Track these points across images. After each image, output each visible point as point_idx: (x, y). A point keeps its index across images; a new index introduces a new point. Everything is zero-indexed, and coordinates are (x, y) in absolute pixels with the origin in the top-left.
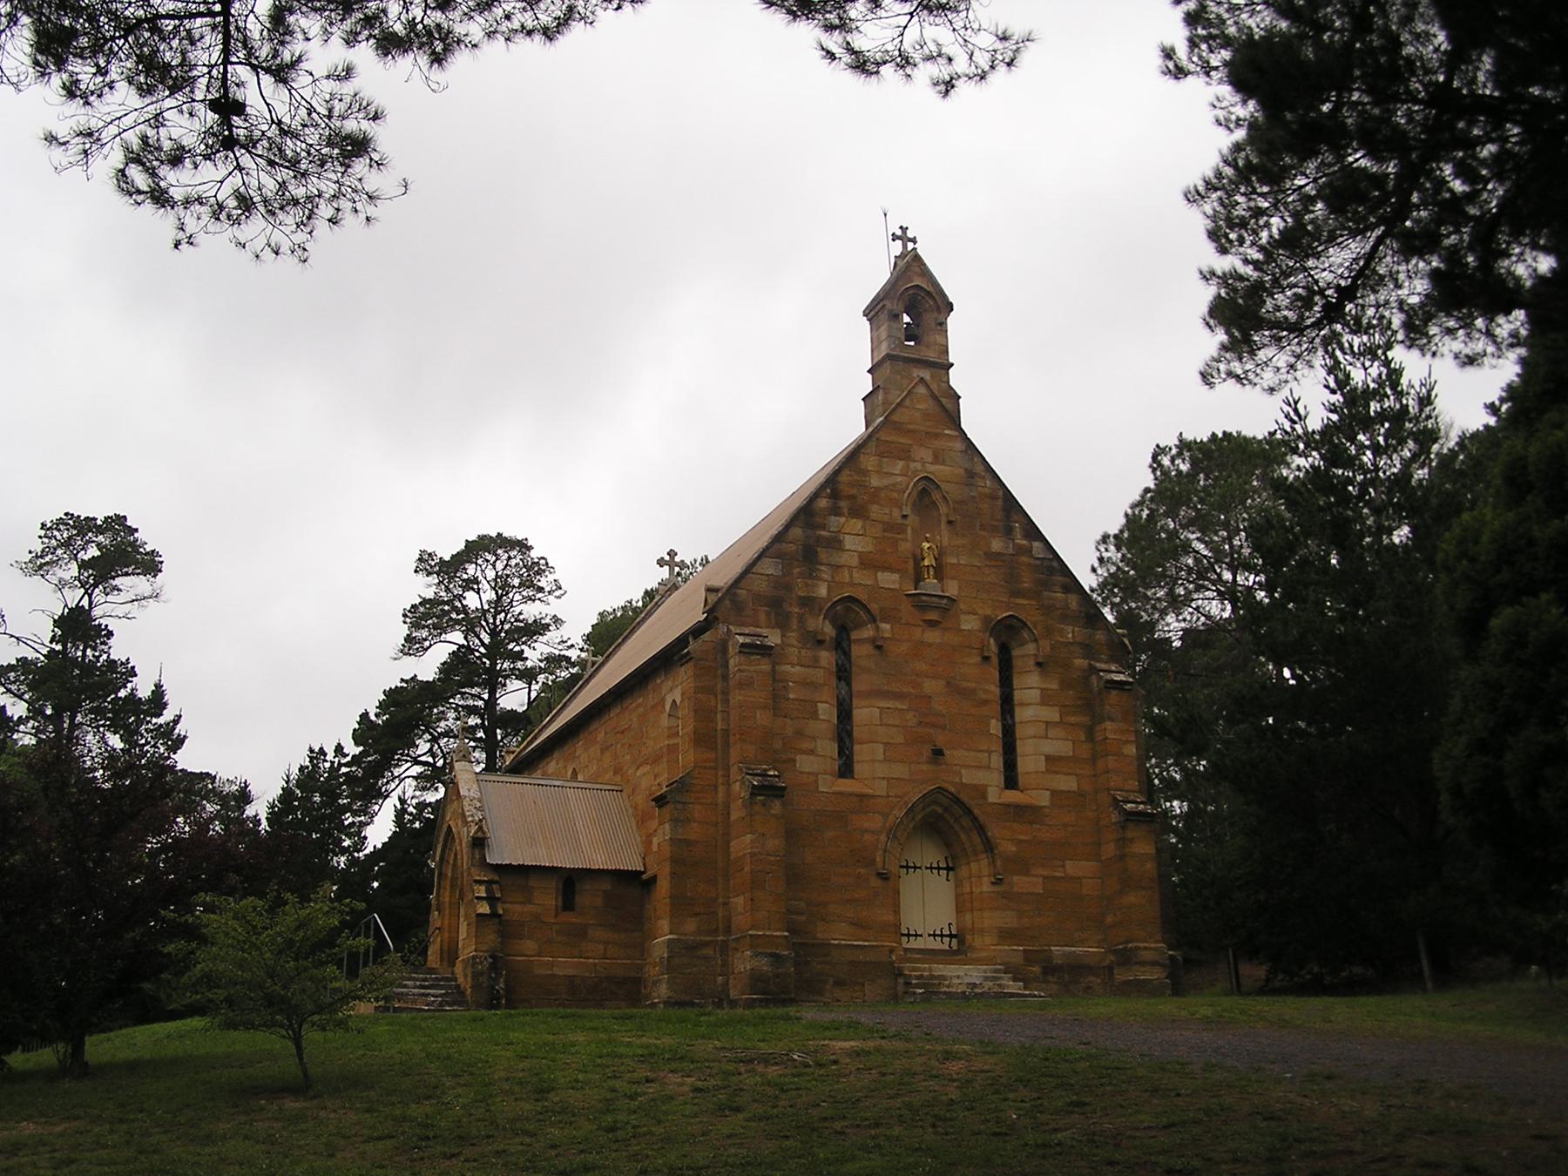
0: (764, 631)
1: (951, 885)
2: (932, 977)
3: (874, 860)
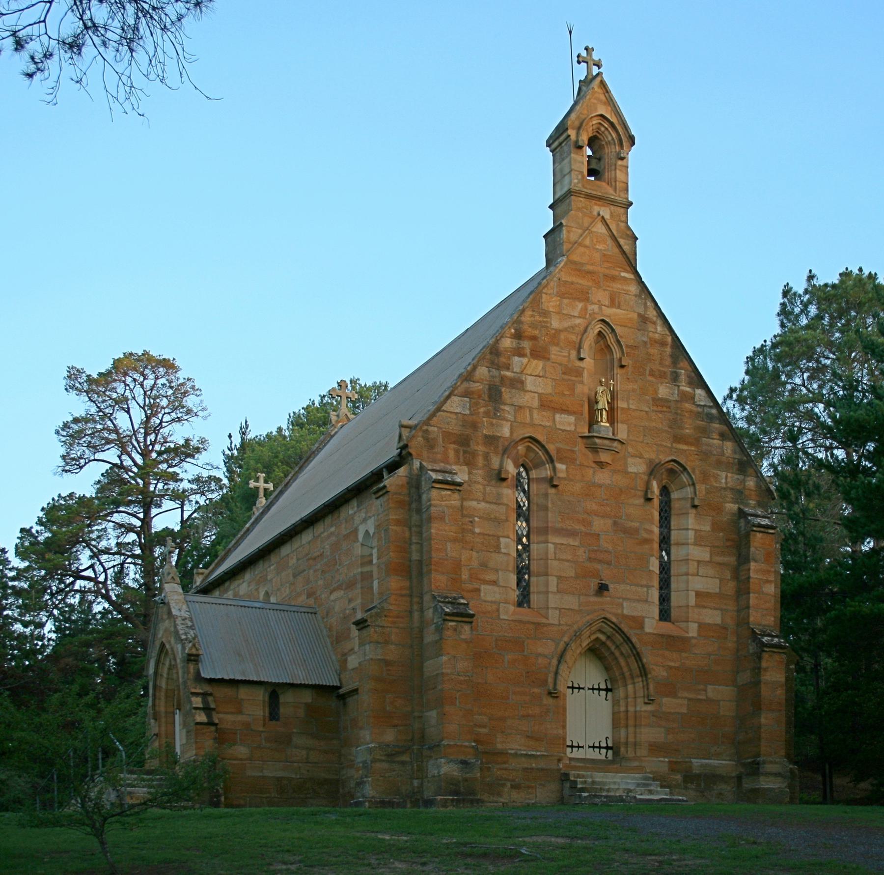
0: (455, 468)
1: (609, 704)
2: (593, 782)
3: (546, 681)
